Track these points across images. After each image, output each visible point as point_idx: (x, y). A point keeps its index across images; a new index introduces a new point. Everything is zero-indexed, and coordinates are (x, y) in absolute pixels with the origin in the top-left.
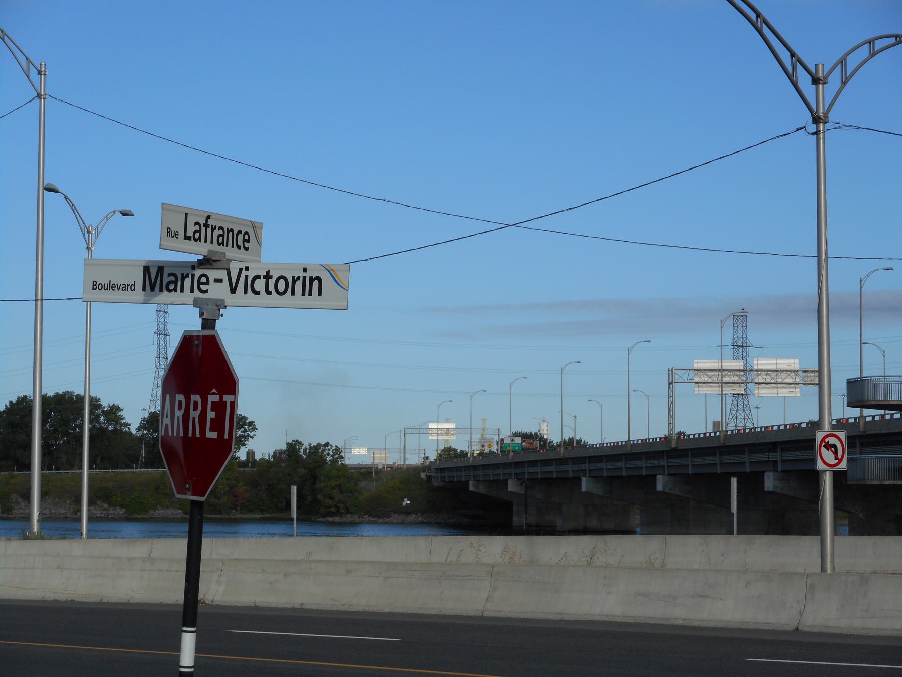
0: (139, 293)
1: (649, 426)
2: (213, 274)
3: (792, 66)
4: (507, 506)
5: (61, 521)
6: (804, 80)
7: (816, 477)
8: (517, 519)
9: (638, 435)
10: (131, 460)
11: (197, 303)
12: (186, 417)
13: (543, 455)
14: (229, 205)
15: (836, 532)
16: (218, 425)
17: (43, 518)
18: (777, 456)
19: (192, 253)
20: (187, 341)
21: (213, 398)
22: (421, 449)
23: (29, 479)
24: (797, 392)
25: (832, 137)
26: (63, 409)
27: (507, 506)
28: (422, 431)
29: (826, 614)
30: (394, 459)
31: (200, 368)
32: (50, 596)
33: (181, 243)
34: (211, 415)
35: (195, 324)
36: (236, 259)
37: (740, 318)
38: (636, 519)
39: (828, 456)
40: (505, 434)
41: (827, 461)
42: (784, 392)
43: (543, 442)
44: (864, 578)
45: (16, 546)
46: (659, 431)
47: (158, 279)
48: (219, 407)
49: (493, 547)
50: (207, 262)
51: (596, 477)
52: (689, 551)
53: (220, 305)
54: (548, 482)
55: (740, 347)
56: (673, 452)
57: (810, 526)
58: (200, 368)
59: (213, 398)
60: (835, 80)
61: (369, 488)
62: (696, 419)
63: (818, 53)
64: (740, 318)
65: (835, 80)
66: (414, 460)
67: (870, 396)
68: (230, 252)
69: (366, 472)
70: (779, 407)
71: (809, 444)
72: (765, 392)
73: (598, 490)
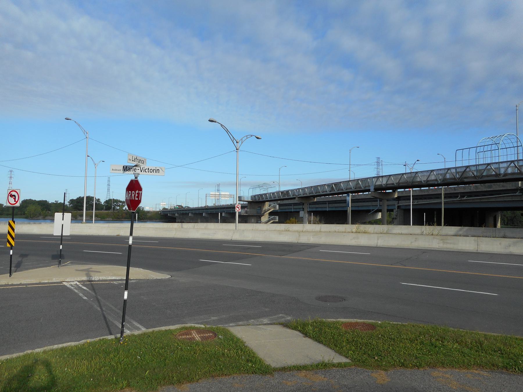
0: (122, 171)
1: (202, 204)
2: (137, 168)
3: (233, 139)
4: (175, 218)
5: (89, 219)
6: (235, 142)
7: (235, 213)
8: (177, 221)
9: (200, 206)
10: (102, 209)
11: (134, 174)
12: (131, 195)
13: (182, 209)
14: (141, 155)
15: (239, 223)
16: (138, 197)
17: (86, 220)
18: (225, 210)
19: (134, 163)
20: (132, 181)
21: (137, 192)
22: (159, 208)
23: (83, 212)
24: (228, 198)
25: (240, 152)
26: (90, 199)
27: (175, 218)
28: (159, 204)
29: (237, 237)
30: (154, 210)
31: (134, 187)
32: (88, 234)
33: (131, 162)
34: (137, 195)
35: (133, 178)
36: (142, 166)
37: (219, 185)
38: (199, 221)
39: (237, 209)
40: (175, 205)
41: (238, 210)
42: (226, 198)
43: (182, 207)
44: (243, 230)
45: (80, 225)
46: (203, 205)
47: (126, 169)
48: (138, 194)
49: (175, 225)
50: (136, 166)
51: (192, 213)
52: (212, 226)
53: (139, 174)
54: (183, 214)
55: (218, 190)
56: (206, 209)
57: (233, 221)
58: (134, 187)
59: (137, 192)
60: (240, 142)
61: (149, 215)
62: (210, 203)
63: (238, 138)
64: (219, 185)
65: (240, 142)
66: (158, 210)
67: (243, 199)
68: (141, 164)
69: (148, 212)
70: (225, 201)
71: (234, 208)
72: (223, 198)
73: (192, 216)
